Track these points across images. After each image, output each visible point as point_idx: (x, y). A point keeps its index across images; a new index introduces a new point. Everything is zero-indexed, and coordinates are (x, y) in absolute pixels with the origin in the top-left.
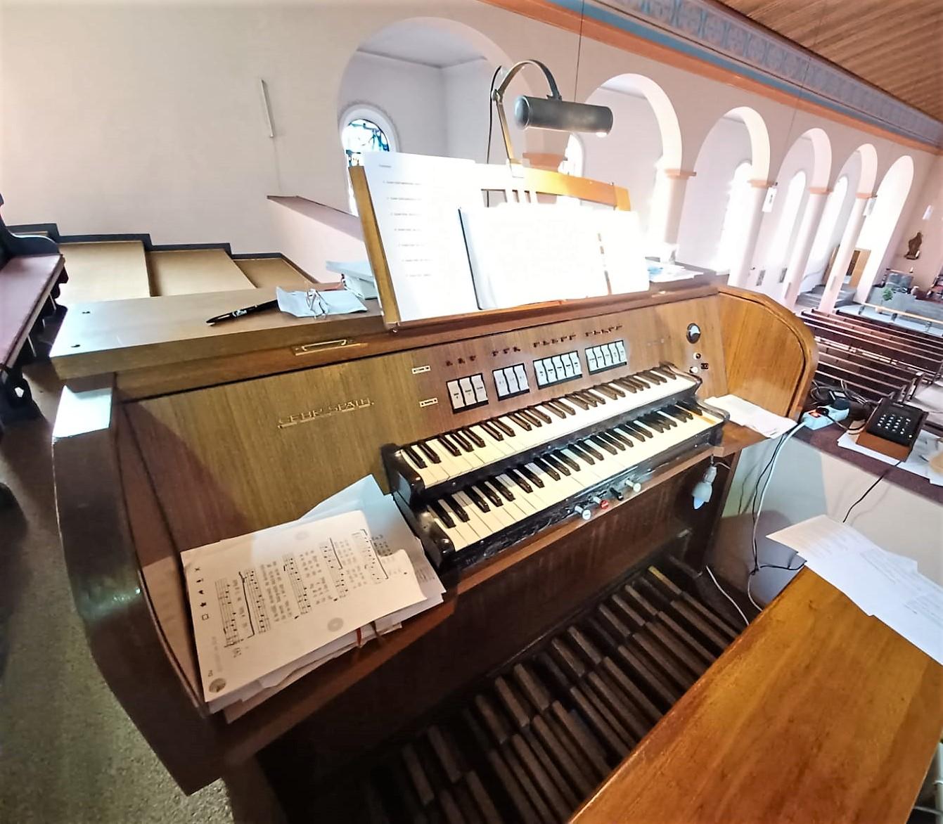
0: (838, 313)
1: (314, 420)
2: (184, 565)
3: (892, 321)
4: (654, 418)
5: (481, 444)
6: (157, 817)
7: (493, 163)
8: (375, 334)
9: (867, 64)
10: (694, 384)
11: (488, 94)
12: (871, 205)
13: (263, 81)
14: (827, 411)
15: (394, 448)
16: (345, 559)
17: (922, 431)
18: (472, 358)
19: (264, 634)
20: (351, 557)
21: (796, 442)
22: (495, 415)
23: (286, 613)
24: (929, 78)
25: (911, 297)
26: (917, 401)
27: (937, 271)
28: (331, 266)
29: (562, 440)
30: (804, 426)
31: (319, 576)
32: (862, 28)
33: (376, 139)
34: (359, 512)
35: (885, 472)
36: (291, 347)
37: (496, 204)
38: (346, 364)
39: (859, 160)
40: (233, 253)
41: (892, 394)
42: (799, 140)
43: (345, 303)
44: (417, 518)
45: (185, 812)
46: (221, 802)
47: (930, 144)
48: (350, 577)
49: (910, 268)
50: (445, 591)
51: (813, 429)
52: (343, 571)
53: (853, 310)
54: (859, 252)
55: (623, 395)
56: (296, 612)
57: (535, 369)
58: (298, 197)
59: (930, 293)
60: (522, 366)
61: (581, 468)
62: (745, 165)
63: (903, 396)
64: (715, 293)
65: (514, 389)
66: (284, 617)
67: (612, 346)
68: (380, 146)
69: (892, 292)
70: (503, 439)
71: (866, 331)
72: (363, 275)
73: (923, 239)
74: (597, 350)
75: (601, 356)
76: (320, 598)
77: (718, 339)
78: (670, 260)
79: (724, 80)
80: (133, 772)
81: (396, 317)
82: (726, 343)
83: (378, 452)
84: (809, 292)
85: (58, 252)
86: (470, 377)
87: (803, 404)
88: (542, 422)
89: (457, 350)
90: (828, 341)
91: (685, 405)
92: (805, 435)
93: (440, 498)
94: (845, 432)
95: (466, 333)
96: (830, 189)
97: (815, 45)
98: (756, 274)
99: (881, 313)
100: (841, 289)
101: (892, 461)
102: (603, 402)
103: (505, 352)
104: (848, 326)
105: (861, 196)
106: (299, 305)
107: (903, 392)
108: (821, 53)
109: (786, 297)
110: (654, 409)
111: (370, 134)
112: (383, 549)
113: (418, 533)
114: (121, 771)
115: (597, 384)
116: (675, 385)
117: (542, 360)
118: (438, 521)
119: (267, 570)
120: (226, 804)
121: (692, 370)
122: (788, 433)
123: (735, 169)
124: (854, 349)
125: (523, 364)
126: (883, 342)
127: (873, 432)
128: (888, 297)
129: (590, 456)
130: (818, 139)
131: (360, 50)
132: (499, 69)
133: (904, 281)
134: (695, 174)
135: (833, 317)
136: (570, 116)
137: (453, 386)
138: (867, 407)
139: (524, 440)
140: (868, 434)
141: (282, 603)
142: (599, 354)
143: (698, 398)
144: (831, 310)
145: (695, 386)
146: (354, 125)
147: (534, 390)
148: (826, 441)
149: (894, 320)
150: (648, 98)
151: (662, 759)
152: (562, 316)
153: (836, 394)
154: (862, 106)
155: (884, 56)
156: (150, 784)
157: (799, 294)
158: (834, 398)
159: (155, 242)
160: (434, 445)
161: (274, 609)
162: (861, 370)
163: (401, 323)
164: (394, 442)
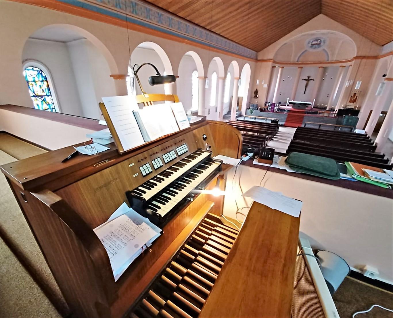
0: (237, 120)
3: (255, 121)
9: (229, 33)
10: (210, 153)
14: (248, 154)
16: (129, 229)
17: (274, 155)
22: (155, 175)
23: (120, 247)
24: (249, 37)
29: (178, 179)
32: (225, 21)
33: (40, 75)
35: (268, 169)
38: (110, 167)
41: (260, 145)
42: (212, 61)
47: (254, 59)
49: (256, 101)
51: (245, 160)
53: (242, 119)
57: (163, 158)
58: (8, 104)
59: (264, 109)
62: (195, 72)
65: (159, 166)
66: (120, 248)
67: (183, 146)
71: (247, 125)
73: (258, 91)
74: (179, 148)
77: (212, 138)
78: (191, 115)
79: (183, 42)
82: (215, 139)
83: (125, 194)
84: (226, 114)
89: (140, 156)
91: (209, 161)
92: (243, 163)
94: (254, 160)
95: (142, 150)
97: (211, 28)
99: (251, 118)
101: (269, 165)
104: (242, 124)
105: (236, 78)
107: (263, 144)
108: (213, 30)
109: (219, 117)
110: (200, 164)
111: (36, 73)
115: (181, 159)
122: (239, 164)
123: (192, 73)
124: (245, 132)
125: (159, 157)
126: (254, 128)
127: (262, 158)
128: (252, 112)
130: (218, 60)
133: (255, 106)
135: (236, 122)
137: (141, 168)
138: (258, 151)
142: (180, 150)
144: (235, 120)
147: (164, 165)
148: (249, 163)
150: (155, 50)
153: (249, 148)
155: (233, 31)
157: (223, 115)
161: (116, 247)
162: (249, 139)
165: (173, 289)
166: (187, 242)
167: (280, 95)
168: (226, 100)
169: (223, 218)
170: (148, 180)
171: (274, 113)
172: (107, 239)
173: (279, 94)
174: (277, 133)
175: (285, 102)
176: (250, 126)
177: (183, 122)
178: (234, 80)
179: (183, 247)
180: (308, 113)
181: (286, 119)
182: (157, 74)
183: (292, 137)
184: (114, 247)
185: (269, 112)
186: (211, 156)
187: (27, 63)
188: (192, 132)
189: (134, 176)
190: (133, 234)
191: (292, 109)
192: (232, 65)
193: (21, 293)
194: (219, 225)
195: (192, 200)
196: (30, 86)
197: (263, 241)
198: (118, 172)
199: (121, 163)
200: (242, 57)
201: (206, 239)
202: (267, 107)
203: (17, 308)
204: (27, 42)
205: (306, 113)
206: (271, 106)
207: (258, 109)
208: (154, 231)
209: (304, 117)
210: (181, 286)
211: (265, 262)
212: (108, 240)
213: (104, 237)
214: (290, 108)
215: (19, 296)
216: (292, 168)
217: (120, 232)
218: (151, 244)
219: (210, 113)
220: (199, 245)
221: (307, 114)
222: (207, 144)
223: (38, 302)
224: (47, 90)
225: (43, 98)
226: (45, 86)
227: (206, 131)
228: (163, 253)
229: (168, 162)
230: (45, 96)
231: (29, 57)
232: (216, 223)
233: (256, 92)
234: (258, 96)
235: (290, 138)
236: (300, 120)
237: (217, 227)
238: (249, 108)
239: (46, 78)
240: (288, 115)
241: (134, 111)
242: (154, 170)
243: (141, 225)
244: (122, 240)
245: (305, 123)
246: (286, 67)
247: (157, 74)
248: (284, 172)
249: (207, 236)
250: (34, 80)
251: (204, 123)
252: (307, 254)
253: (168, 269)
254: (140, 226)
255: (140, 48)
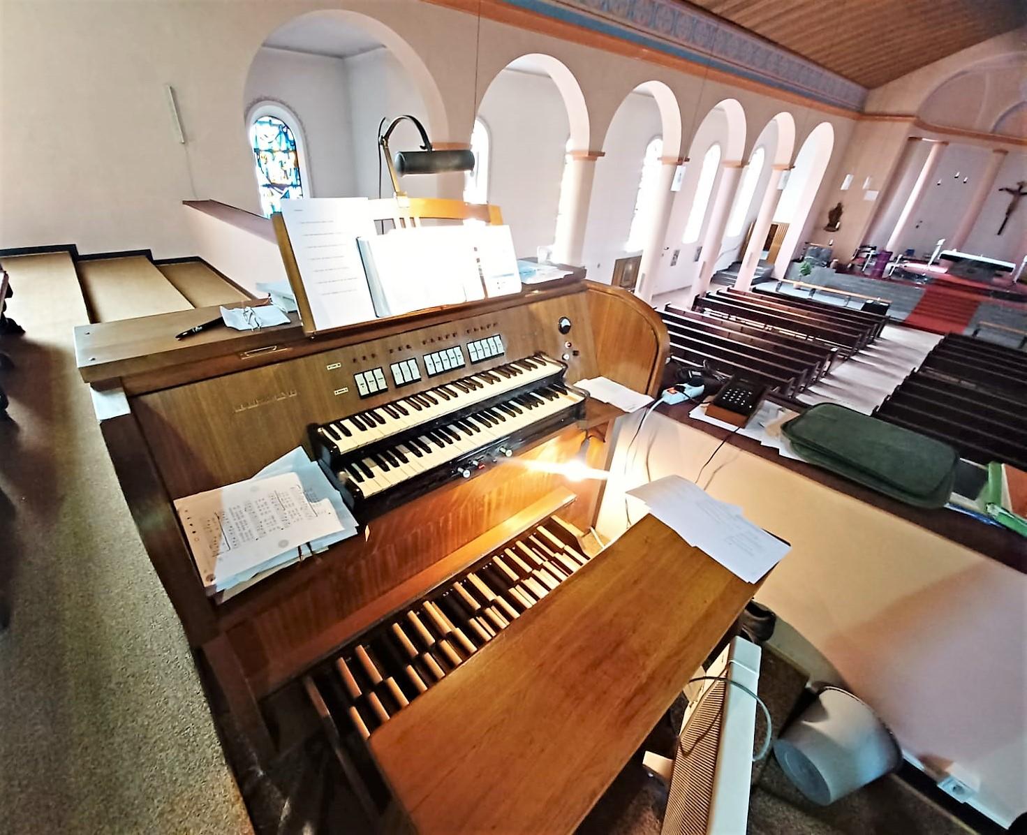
0: (755, 290)
1: (258, 407)
2: (177, 509)
3: (810, 297)
4: (526, 397)
5: (382, 421)
6: (151, 715)
7: (384, 198)
8: (296, 340)
10: (560, 369)
11: (376, 140)
12: (785, 177)
13: (171, 88)
15: (316, 426)
18: (373, 356)
19: (237, 549)
20: (290, 503)
21: (658, 416)
22: (394, 400)
23: (250, 536)
25: (831, 270)
26: (832, 377)
27: (858, 244)
28: (260, 286)
30: (663, 402)
31: (270, 514)
33: (283, 136)
34: (293, 473)
35: (728, 437)
36: (237, 354)
37: (386, 233)
38: (278, 364)
39: (776, 130)
40: (154, 259)
41: (805, 371)
43: (273, 317)
44: (337, 476)
45: (173, 709)
46: (200, 701)
47: (853, 110)
48: (291, 515)
49: (830, 240)
50: (358, 525)
51: (671, 404)
52: (286, 511)
53: (770, 287)
54: (777, 226)
55: (499, 380)
56: (256, 535)
58: (211, 200)
59: (850, 265)
60: (414, 360)
61: (461, 438)
63: (817, 372)
64: (584, 289)
65: (408, 379)
68: (287, 142)
69: (811, 266)
70: (399, 418)
71: (783, 309)
72: (286, 295)
73: (843, 209)
74: (477, 344)
75: (482, 349)
76: (272, 527)
77: (588, 330)
79: (632, 54)
80: (130, 685)
81: (313, 328)
82: (596, 333)
85: (2, 269)
86: (372, 371)
87: (659, 381)
88: (431, 404)
89: (360, 350)
90: (743, 320)
91: (553, 386)
92: (664, 409)
93: (353, 463)
94: (698, 405)
96: (744, 162)
98: (670, 254)
99: (799, 289)
100: (758, 266)
102: (482, 386)
103: (400, 349)
104: (764, 304)
106: (240, 321)
107: (817, 368)
108: (733, 18)
109: (700, 276)
110: (527, 391)
111: (276, 130)
112: (312, 497)
113: (337, 487)
114: (119, 685)
116: (551, 369)
117: (431, 354)
118: (352, 478)
119: (234, 511)
120: (204, 702)
121: (564, 357)
124: (769, 327)
126: (800, 319)
128: (806, 272)
129: (469, 429)
130: (731, 111)
131: (264, 45)
132: (384, 119)
134: (603, 154)
136: (438, 162)
137: (359, 378)
139: (415, 418)
140: (716, 407)
141: (246, 531)
143: (565, 381)
144: (747, 288)
145: (561, 371)
146: (260, 122)
148: (680, 413)
149: (812, 296)
151: (517, 638)
152: (448, 317)
154: (778, 73)
156: (145, 692)
158: (691, 377)
159: (82, 252)
160: (347, 423)
161: (241, 534)
162: (776, 348)
163: (317, 332)
164: (316, 422)
165: (407, 658)
166: (477, 568)
167: (917, 227)
168: (735, 231)
169: (594, 536)
170: (372, 407)
171: (880, 282)
172: (232, 514)
173: (915, 223)
174: (872, 342)
175: (928, 252)
176: (789, 310)
177: (503, 278)
178: (771, 172)
179: (462, 577)
180: (997, 295)
181: (915, 305)
182: (421, 147)
183: (921, 360)
184: (238, 533)
185: (866, 276)
186: (564, 376)
187: (261, 106)
188: (528, 308)
189: (337, 393)
190: (289, 517)
191: (948, 275)
192: (776, 127)
193: (136, 577)
194: (568, 549)
195: (467, 474)
196: (263, 161)
197: (616, 615)
198: (294, 375)
199: (306, 358)
200: (810, 101)
201: (523, 575)
202: (863, 261)
203: (121, 603)
204: (258, 58)
205: (989, 296)
206: (876, 259)
207: (828, 265)
208: (338, 522)
209: (980, 307)
210: (428, 656)
211: (596, 664)
212: (233, 516)
213: (230, 509)
214: (940, 271)
215: (131, 582)
216: (797, 448)
217: (265, 507)
218: (328, 549)
219: (677, 263)
220: (501, 584)
221: (991, 299)
222: (567, 345)
223: (157, 603)
224: (293, 172)
225: (284, 192)
226: (290, 165)
227: (575, 308)
228: (410, 577)
229: (437, 374)
230: (288, 186)
231: (275, 96)
232: (560, 544)
233: (836, 214)
234: (840, 226)
235: (910, 361)
236: (966, 312)
237: (562, 554)
238: (801, 258)
239: (295, 144)
240: (929, 291)
241: (359, 239)
242: (394, 386)
243: (318, 503)
244: (261, 524)
245: (979, 325)
246: (956, 143)
247: (421, 147)
248: (771, 454)
249: (528, 569)
250: (270, 148)
251: (575, 286)
252: (735, 683)
253: (413, 615)
254: (314, 504)
255: (520, 74)
